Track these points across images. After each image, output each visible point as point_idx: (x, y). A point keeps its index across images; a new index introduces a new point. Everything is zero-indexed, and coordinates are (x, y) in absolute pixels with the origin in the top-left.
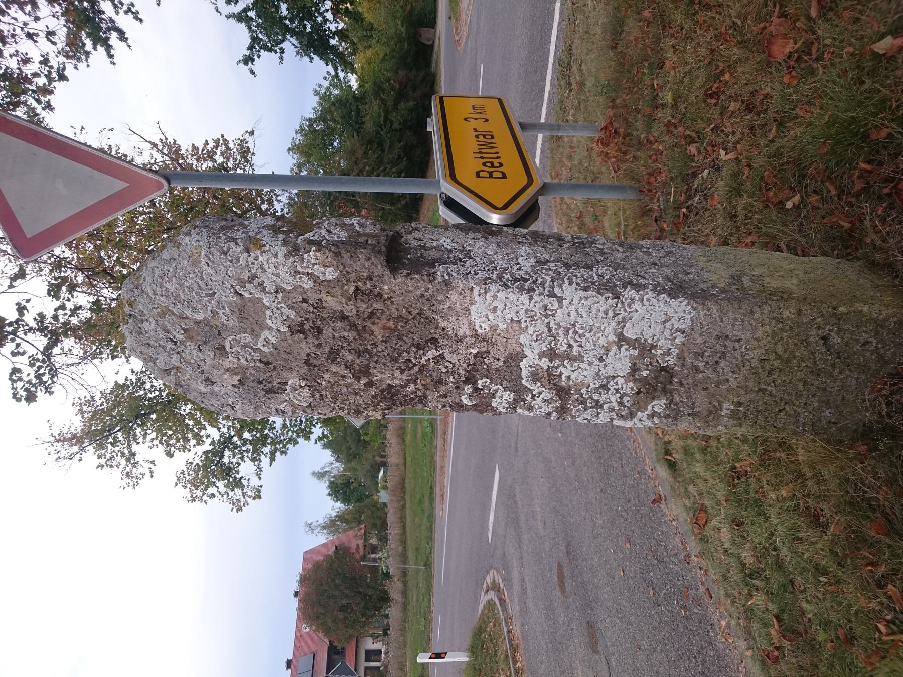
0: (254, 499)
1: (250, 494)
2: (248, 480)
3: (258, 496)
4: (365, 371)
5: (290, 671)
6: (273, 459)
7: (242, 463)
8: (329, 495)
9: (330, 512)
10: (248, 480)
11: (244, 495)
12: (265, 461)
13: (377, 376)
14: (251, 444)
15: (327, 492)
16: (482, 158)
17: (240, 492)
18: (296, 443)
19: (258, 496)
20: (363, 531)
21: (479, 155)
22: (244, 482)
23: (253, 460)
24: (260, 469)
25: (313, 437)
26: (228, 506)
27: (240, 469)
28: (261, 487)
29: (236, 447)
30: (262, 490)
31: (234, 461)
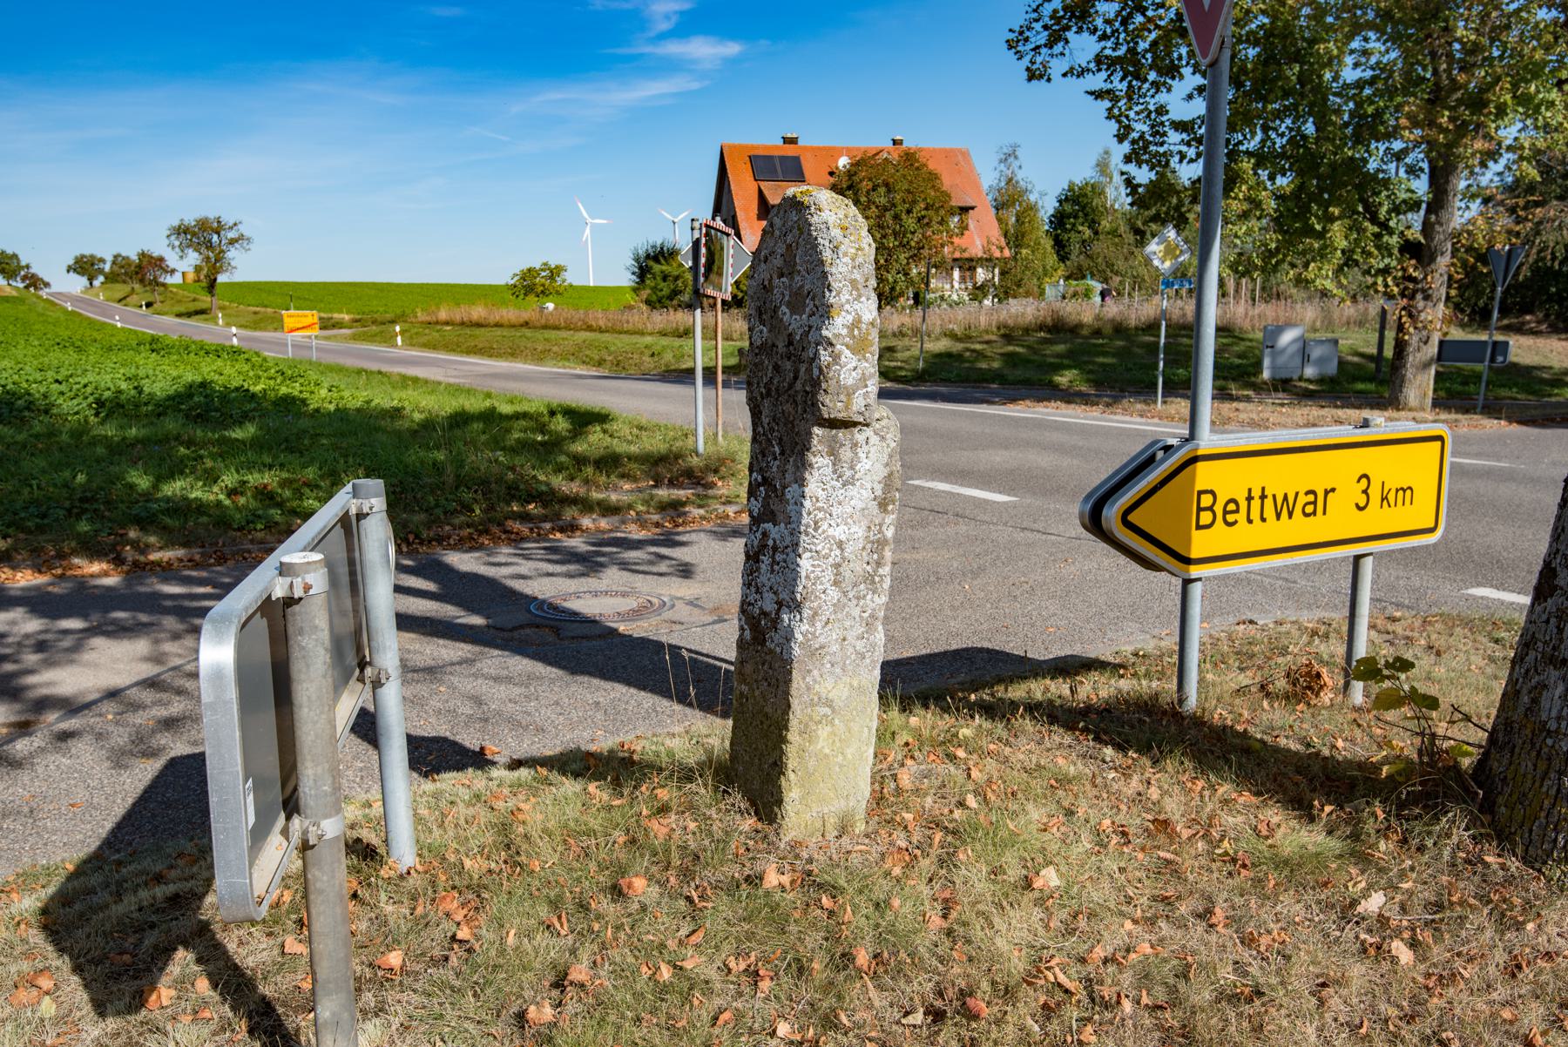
0: (1028, 69)
1: (1039, 59)
2: (1062, 54)
3: (1032, 75)
4: (768, 394)
5: (781, 142)
6: (1098, 95)
7: (1095, 38)
8: (1071, 189)
9: (1038, 188)
10: (1062, 54)
11: (1036, 49)
12: (1097, 81)
13: (766, 403)
14: (1129, 50)
15: (1077, 181)
16: (1249, 498)
17: (1043, 42)
18: (1121, 138)
19: (1032, 75)
20: (997, 254)
21: (1256, 493)
22: (1058, 48)
23: (1099, 60)
24: (1080, 74)
25: (1131, 168)
26: (1018, 21)
27: (1085, 34)
28: (1049, 80)
29: (1124, 22)
30: (1043, 81)
31: (1099, 22)
